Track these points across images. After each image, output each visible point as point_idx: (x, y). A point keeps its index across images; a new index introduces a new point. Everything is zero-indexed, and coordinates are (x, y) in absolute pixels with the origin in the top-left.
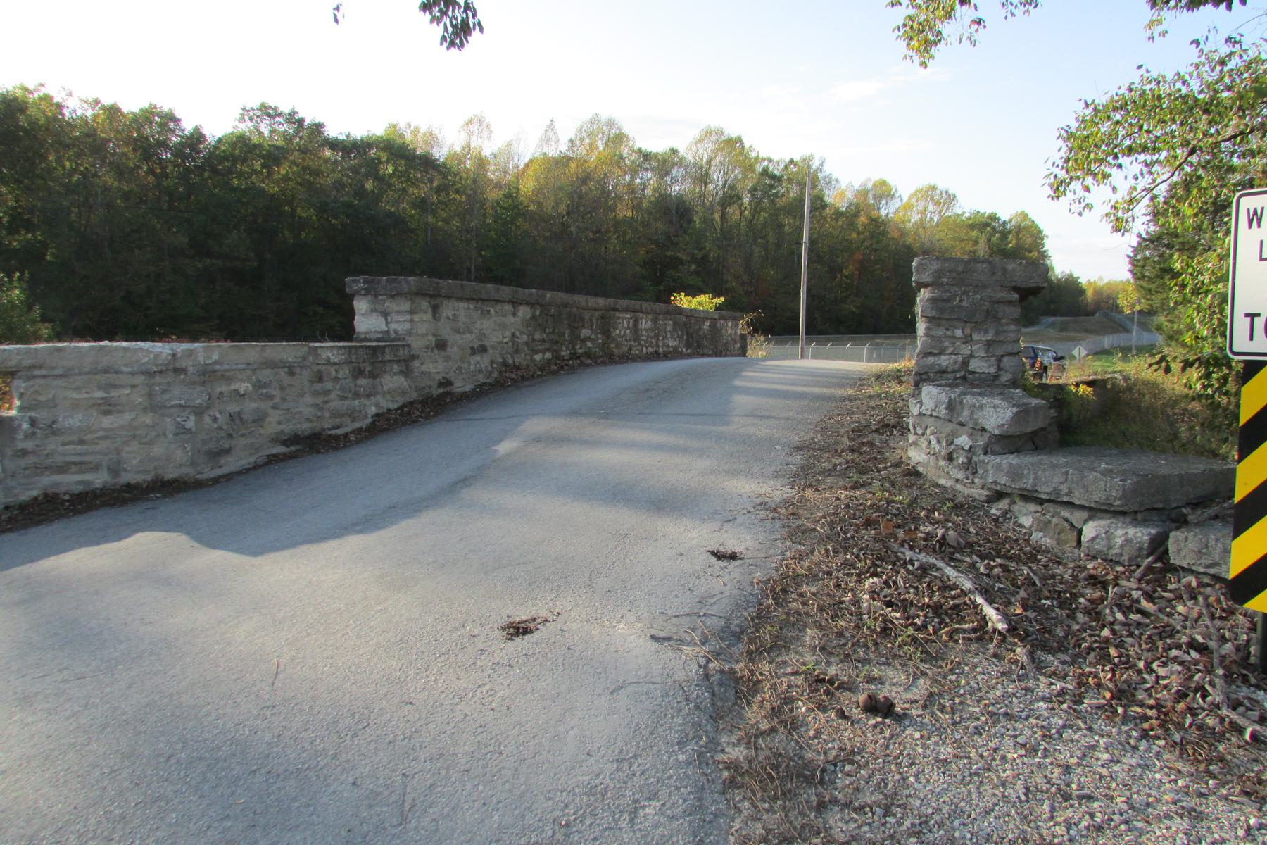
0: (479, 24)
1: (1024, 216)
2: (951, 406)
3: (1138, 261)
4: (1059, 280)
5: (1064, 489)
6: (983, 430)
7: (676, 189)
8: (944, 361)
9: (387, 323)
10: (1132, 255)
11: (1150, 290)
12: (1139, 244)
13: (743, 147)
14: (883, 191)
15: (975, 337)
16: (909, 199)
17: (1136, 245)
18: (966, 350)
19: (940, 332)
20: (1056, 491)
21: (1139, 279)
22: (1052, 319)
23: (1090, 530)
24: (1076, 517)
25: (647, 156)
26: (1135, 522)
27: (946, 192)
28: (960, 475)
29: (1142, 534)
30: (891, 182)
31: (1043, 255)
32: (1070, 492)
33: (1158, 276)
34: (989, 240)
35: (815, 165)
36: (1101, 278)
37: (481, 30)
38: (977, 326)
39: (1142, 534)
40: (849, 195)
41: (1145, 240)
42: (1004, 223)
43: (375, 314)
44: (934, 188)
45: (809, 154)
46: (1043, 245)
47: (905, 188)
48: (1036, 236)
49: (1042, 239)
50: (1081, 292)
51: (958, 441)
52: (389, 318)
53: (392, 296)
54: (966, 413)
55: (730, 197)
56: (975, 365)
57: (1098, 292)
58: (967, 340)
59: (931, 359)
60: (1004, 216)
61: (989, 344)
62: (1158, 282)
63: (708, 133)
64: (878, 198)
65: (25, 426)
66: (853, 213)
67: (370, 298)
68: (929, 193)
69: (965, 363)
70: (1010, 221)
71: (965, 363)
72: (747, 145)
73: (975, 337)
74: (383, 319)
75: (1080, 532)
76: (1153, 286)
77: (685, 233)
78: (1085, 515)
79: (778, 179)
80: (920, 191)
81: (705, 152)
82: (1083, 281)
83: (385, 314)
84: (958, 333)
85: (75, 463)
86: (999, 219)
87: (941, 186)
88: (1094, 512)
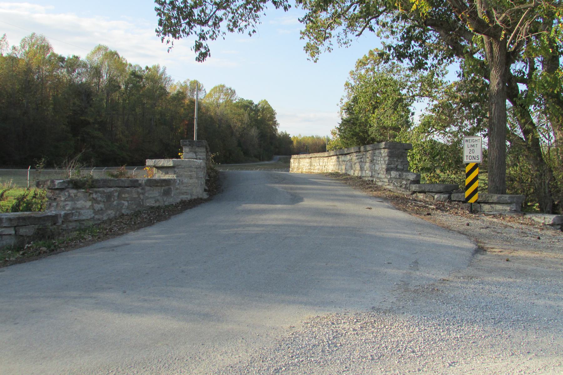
0: (210, 54)
1: (266, 102)
2: (400, 175)
3: (342, 130)
4: (280, 136)
5: (431, 189)
6: (409, 180)
7: (78, 80)
8: (392, 166)
9: (196, 156)
10: (339, 127)
11: (347, 144)
12: (342, 122)
13: (119, 58)
14: (196, 86)
15: (399, 160)
16: (211, 91)
17: (340, 123)
18: (397, 164)
19: (391, 159)
20: (429, 190)
21: (343, 138)
22: (278, 157)
23: (436, 196)
24: (433, 194)
25: (62, 59)
26: (444, 194)
27: (230, 89)
28: (404, 190)
29: (447, 196)
30: (201, 82)
31: (275, 123)
32: (432, 190)
33: (350, 137)
34: (249, 115)
35: (161, 70)
36: (300, 135)
37: (210, 56)
38: (399, 158)
39: (447, 196)
40: (178, 88)
41: (345, 120)
42: (256, 106)
43: (191, 153)
44: (224, 86)
45: (157, 65)
46: (275, 118)
47: (208, 86)
48: (272, 113)
49: (274, 115)
50: (291, 142)
51: (403, 182)
52: (197, 154)
53: (199, 147)
54: (404, 176)
55: (113, 86)
56: (399, 167)
57: (299, 142)
58: (397, 161)
59: (390, 166)
60: (256, 103)
61: (402, 162)
62: (351, 140)
63: (99, 48)
64: (193, 90)
65: (178, 181)
66: (180, 96)
67: (190, 147)
68: (221, 89)
69: (397, 166)
70: (259, 104)
71: (397, 166)
72: (121, 56)
73: (399, 160)
74: (195, 154)
75: (434, 197)
76: (349, 142)
77: (91, 106)
78: (435, 194)
79: (140, 77)
80: (216, 88)
81: (97, 59)
82: (291, 136)
83: (195, 153)
84: (395, 159)
85: (186, 192)
86: (253, 103)
87: (228, 86)
88: (437, 193)
